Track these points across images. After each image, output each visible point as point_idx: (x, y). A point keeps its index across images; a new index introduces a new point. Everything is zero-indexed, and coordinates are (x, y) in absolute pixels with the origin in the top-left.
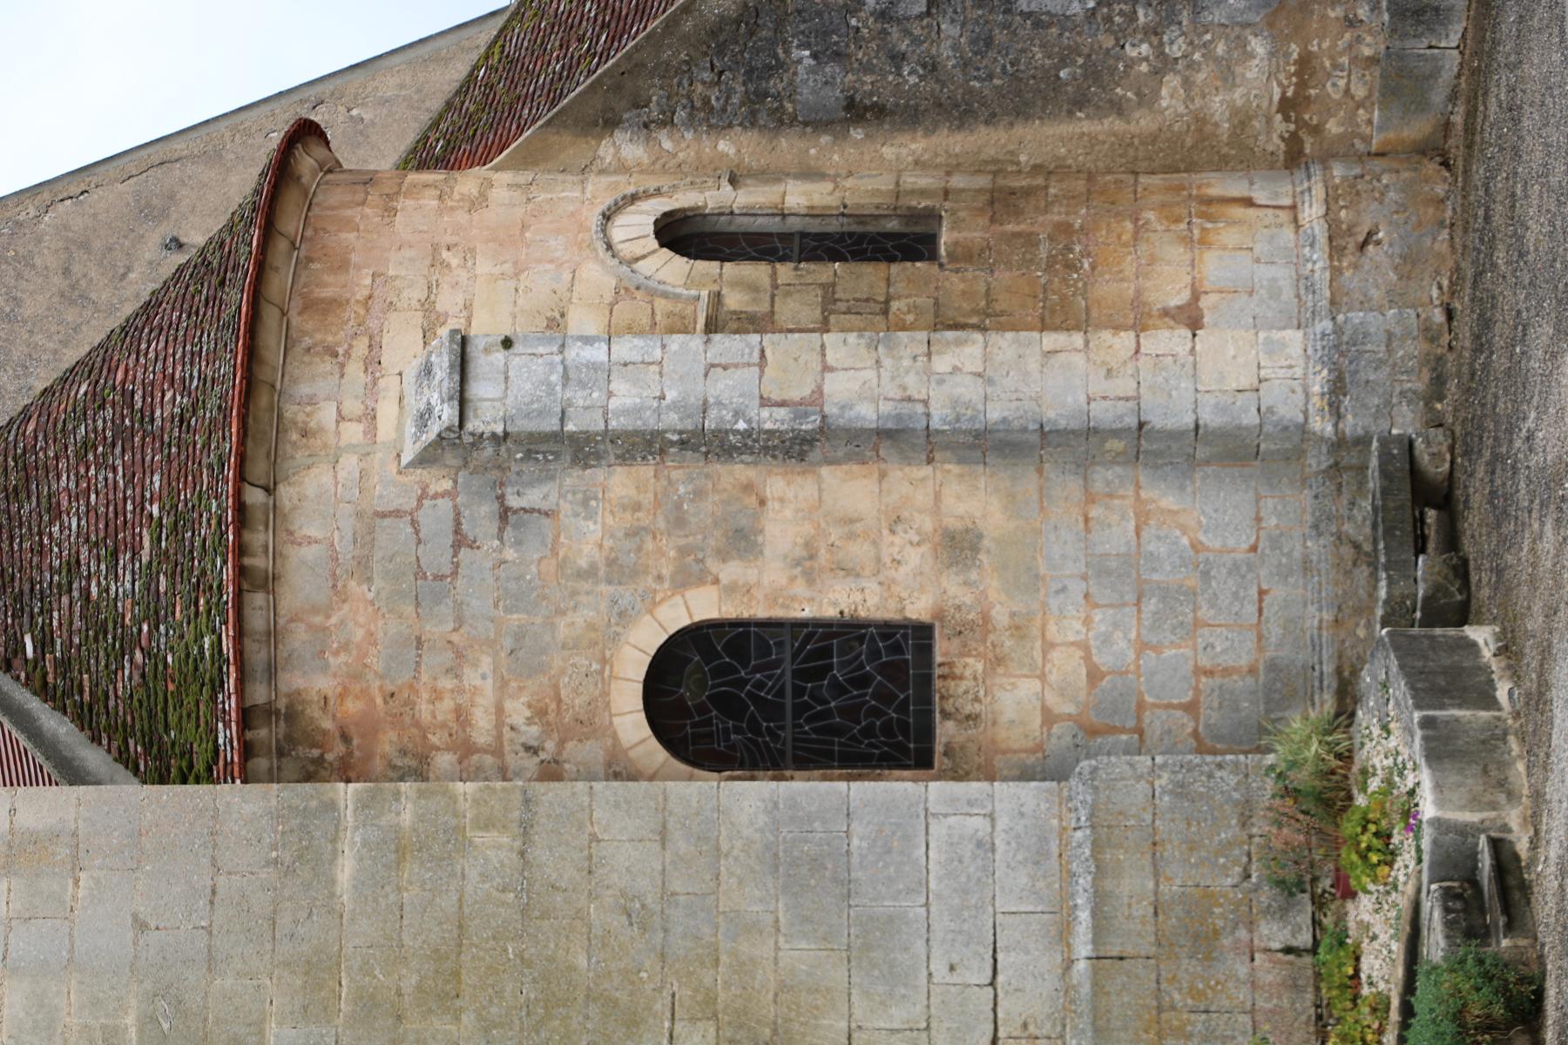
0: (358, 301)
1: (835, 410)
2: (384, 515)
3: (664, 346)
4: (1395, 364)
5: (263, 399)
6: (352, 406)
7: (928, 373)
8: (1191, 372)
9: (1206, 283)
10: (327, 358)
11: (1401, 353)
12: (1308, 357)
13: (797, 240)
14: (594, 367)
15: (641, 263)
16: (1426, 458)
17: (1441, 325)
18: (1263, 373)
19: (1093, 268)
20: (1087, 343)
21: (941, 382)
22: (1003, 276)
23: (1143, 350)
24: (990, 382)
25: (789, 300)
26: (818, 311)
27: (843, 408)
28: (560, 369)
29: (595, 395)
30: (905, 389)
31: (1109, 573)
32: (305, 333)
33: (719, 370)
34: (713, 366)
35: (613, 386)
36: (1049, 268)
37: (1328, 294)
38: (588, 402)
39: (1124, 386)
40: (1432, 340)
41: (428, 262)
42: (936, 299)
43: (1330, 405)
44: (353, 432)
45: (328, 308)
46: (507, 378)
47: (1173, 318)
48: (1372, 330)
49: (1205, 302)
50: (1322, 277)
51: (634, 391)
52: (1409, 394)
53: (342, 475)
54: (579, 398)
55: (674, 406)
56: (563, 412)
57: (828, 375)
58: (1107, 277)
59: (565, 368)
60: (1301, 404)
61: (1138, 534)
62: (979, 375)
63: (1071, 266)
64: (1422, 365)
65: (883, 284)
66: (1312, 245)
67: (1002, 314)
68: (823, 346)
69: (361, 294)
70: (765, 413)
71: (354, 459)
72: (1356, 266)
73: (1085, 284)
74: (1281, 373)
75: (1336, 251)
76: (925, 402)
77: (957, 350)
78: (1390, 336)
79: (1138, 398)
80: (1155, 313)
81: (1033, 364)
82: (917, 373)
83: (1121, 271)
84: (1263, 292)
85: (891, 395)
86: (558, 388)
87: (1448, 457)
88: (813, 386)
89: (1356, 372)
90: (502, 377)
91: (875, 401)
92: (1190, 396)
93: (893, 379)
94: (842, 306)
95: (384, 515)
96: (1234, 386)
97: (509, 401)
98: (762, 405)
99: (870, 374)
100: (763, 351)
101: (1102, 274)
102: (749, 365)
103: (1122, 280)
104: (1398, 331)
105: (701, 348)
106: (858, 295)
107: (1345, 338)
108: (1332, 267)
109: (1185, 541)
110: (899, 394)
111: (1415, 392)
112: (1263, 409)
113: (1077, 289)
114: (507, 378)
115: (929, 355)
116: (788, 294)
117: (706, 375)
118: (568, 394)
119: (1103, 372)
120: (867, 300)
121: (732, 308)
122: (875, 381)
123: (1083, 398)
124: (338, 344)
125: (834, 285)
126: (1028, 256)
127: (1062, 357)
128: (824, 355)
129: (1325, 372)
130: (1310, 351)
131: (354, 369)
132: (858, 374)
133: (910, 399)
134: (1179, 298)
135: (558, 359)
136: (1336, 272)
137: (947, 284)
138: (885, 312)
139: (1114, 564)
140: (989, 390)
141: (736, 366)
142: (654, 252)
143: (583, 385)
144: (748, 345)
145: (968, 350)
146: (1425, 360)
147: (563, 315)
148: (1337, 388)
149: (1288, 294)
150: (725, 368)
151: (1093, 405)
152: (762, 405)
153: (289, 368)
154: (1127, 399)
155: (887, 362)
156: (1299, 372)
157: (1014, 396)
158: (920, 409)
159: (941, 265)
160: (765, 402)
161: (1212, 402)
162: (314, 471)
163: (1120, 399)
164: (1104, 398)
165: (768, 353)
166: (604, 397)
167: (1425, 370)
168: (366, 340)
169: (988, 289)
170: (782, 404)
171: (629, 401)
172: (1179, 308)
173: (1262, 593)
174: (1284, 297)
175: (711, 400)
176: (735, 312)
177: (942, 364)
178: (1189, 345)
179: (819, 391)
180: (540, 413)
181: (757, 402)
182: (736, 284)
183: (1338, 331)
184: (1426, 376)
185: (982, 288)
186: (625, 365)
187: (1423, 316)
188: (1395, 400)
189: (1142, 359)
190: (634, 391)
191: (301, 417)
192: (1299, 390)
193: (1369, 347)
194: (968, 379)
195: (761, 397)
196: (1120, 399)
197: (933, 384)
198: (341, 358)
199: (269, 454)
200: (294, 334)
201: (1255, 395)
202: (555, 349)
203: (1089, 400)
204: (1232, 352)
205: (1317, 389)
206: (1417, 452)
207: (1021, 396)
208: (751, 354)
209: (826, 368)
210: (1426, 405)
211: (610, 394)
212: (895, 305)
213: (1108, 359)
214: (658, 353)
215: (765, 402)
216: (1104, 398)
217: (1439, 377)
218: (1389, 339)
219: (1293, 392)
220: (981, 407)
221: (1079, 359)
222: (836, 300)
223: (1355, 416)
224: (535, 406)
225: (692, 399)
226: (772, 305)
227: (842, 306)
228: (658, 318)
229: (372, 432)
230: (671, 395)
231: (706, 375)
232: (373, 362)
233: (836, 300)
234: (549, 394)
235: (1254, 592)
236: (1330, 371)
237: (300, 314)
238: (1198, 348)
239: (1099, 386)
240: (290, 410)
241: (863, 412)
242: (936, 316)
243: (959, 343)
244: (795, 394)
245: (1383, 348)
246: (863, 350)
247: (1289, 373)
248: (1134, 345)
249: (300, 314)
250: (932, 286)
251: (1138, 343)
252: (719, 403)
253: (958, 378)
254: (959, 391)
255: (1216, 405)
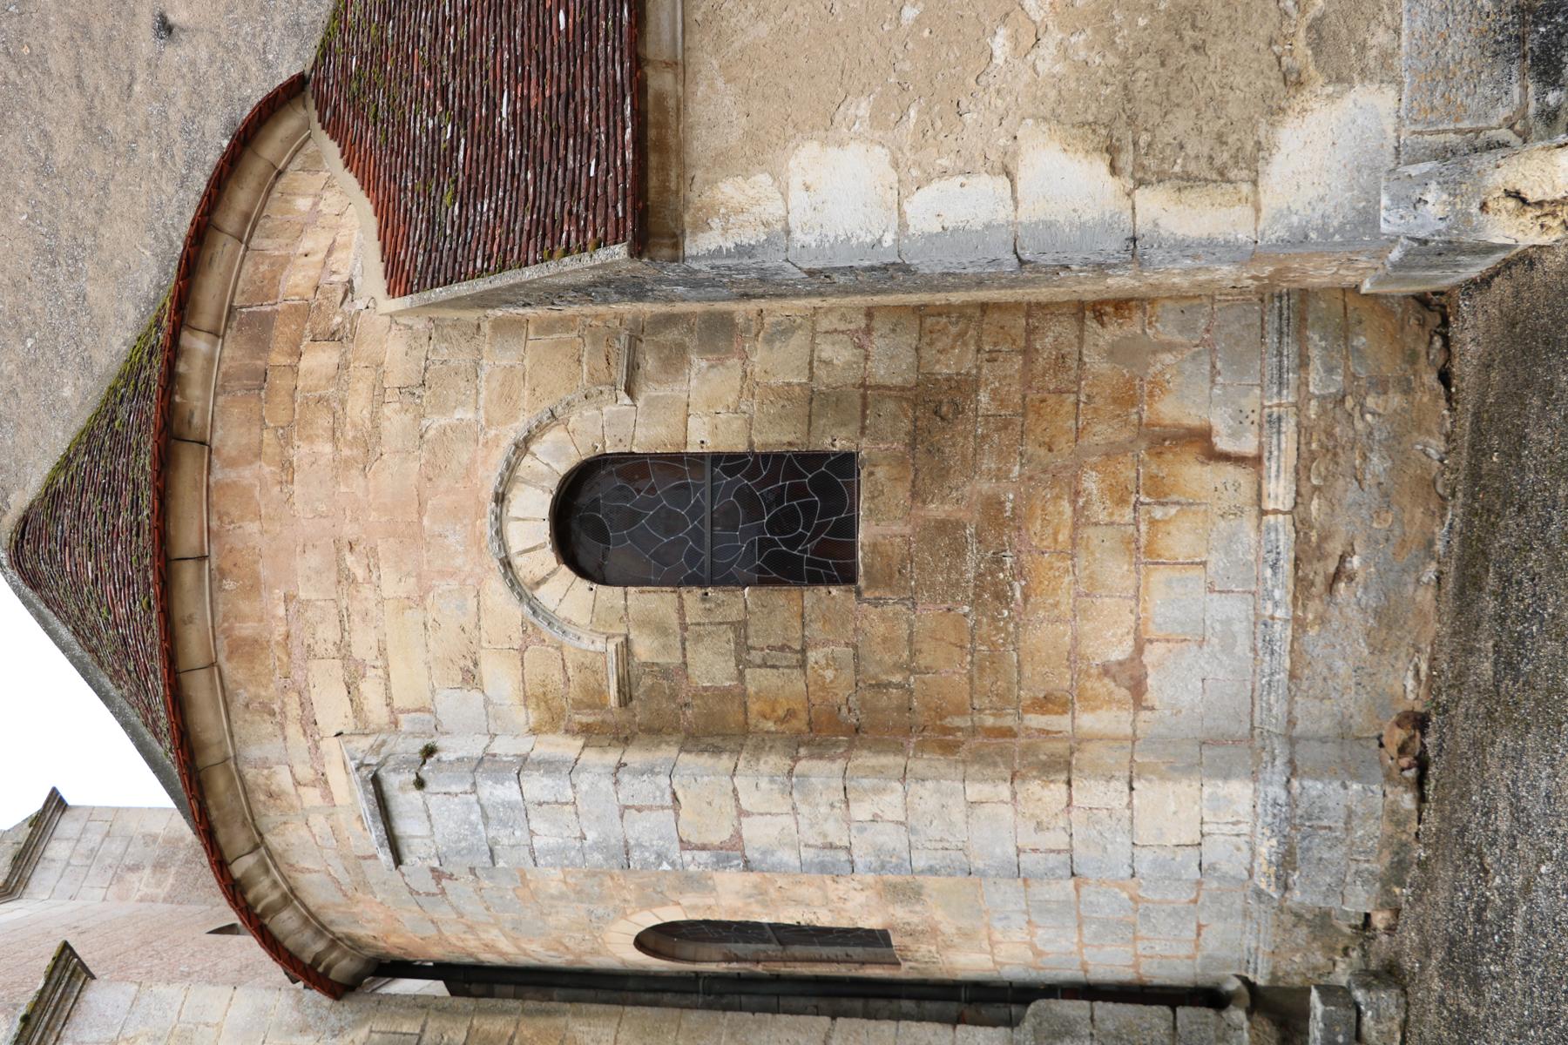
0: (277, 643)
1: (757, 856)
2: (365, 858)
3: (574, 786)
4: (1353, 843)
5: (219, 782)
6: (305, 772)
7: (848, 821)
8: (1127, 826)
9: (1152, 627)
10: (266, 717)
11: (1360, 833)
12: (1257, 815)
13: (708, 464)
14: (510, 806)
15: (543, 588)
16: (1374, 1034)
17: (1410, 811)
18: (1206, 829)
19: (1026, 597)
20: (1014, 795)
21: (862, 830)
22: (928, 614)
23: (1075, 803)
24: (912, 830)
25: (700, 647)
26: (732, 663)
27: (764, 853)
28: (477, 808)
29: (518, 833)
30: (825, 836)
31: (1049, 911)
32: (239, 685)
33: (633, 811)
34: (627, 807)
35: (533, 825)
36: (976, 602)
37: (1287, 664)
38: (512, 841)
39: (1058, 839)
40: (1398, 824)
41: (333, 577)
42: (855, 647)
43: (1278, 878)
44: (312, 796)
45: (249, 649)
46: (429, 816)
47: (1114, 678)
48: (1331, 804)
49: (1152, 654)
50: (1282, 632)
51: (554, 831)
52: (1366, 875)
53: (316, 830)
54: (504, 837)
55: (596, 847)
56: (491, 850)
57: (744, 820)
58: (1041, 613)
59: (482, 807)
60: (1246, 862)
61: (1077, 890)
62: (902, 823)
63: (1001, 597)
64: (1383, 846)
65: (797, 624)
66: (1274, 567)
67: (927, 670)
68: (735, 790)
69: (278, 636)
70: (687, 856)
71: (321, 818)
72: (1322, 620)
73: (1017, 626)
74: (1227, 829)
75: (1302, 585)
76: (848, 849)
77: (876, 799)
78: (1350, 814)
79: (1070, 850)
80: (1094, 671)
81: (957, 813)
82: (837, 820)
83: (1056, 605)
84: (1215, 641)
85: (811, 842)
86: (481, 827)
87: (1398, 1036)
88: (731, 831)
89: (1309, 849)
90: (424, 816)
91: (796, 847)
92: (1127, 850)
93: (812, 826)
94: (756, 656)
95: (365, 858)
96: (1175, 842)
97: (438, 837)
98: (683, 849)
99: (788, 821)
100: (674, 794)
101: (1035, 612)
102: (663, 808)
103: (1058, 620)
104: (1360, 809)
105: (612, 788)
106: (771, 642)
107: (1299, 812)
108: (1296, 619)
109: (1125, 895)
110: (820, 842)
111: (1371, 873)
112: (1204, 866)
113: (1008, 634)
114: (429, 816)
115: (847, 802)
116: (699, 638)
117: (622, 817)
118: (492, 833)
119: (1033, 824)
120: (782, 648)
121: (643, 659)
122: (794, 827)
123: (1012, 851)
124: (271, 700)
125: (744, 624)
126: (954, 576)
127: (988, 808)
128: (737, 800)
129: (1274, 842)
130: (1259, 809)
131: (293, 730)
132: (775, 819)
133: (831, 846)
134: (1119, 652)
135: (473, 798)
136: (1299, 624)
137: (866, 624)
138: (803, 665)
139: (1054, 906)
140: (913, 839)
141: (650, 808)
142: (553, 572)
143: (503, 823)
144: (658, 787)
145: (887, 798)
146: (1387, 842)
147: (476, 664)
148: (1287, 862)
149: (1243, 646)
150: (639, 810)
151: (1022, 857)
152: (683, 849)
153: (235, 729)
154: (1059, 852)
155: (803, 809)
156: (1245, 828)
157: (940, 845)
158: (843, 856)
159: (859, 593)
160: (685, 845)
161: (1150, 857)
162: (290, 827)
163: (1052, 851)
164: (1035, 850)
165: (680, 795)
166: (527, 836)
167: (1386, 852)
168: (295, 697)
169: (911, 634)
170: (703, 848)
171: (552, 841)
172: (1120, 663)
173: (1199, 927)
174: (1238, 650)
175: (632, 842)
176: (645, 664)
177: (861, 811)
178: (1126, 800)
179: (738, 835)
180: (470, 851)
181: (677, 845)
182: (645, 623)
183: (1292, 803)
184: (1387, 859)
185: (903, 631)
186: (540, 804)
187: (1390, 797)
188: (1348, 879)
189: (1075, 812)
190: (554, 831)
191: (261, 780)
192: (1245, 848)
193: (1325, 823)
194: (890, 827)
195: (681, 841)
196: (1052, 851)
197: (854, 832)
198: (279, 718)
199: (244, 824)
200: (230, 686)
201: (1194, 852)
202: (468, 787)
203: (1019, 851)
204: (1173, 808)
205: (1263, 850)
206: (1364, 1030)
207: (947, 845)
208: (663, 796)
209: (742, 813)
210: (1383, 886)
211: (532, 833)
212: (813, 656)
213: (1038, 812)
214: (569, 793)
215: (685, 845)
216: (1035, 850)
217: (1400, 862)
218: (1349, 816)
219: (1238, 849)
220: (906, 856)
221: (1007, 812)
222: (750, 648)
223: (1303, 892)
224: (463, 844)
225: (613, 841)
226: (685, 656)
227: (756, 656)
228: (570, 672)
229: (328, 795)
230: (591, 836)
231: (622, 817)
232: (309, 723)
233: (750, 648)
234: (474, 834)
235: (1194, 926)
236: (1279, 843)
237: (228, 659)
238: (1135, 802)
239: (1029, 839)
240: (250, 774)
241: (785, 858)
242: (857, 672)
243: (877, 791)
244: (715, 839)
245: (1341, 824)
246: (777, 796)
247: (1236, 829)
248: (1065, 799)
249: (228, 659)
250: (851, 627)
251: (1070, 796)
252: (640, 845)
253: (879, 826)
254: (881, 839)
255: (1155, 861)
